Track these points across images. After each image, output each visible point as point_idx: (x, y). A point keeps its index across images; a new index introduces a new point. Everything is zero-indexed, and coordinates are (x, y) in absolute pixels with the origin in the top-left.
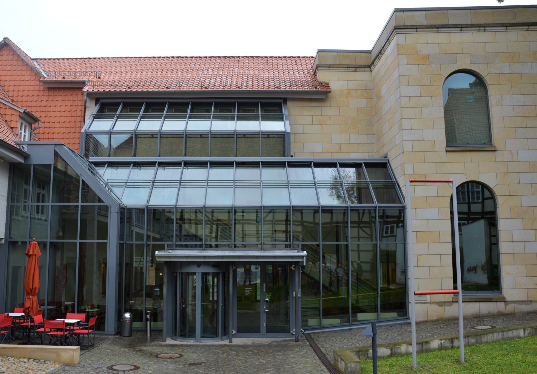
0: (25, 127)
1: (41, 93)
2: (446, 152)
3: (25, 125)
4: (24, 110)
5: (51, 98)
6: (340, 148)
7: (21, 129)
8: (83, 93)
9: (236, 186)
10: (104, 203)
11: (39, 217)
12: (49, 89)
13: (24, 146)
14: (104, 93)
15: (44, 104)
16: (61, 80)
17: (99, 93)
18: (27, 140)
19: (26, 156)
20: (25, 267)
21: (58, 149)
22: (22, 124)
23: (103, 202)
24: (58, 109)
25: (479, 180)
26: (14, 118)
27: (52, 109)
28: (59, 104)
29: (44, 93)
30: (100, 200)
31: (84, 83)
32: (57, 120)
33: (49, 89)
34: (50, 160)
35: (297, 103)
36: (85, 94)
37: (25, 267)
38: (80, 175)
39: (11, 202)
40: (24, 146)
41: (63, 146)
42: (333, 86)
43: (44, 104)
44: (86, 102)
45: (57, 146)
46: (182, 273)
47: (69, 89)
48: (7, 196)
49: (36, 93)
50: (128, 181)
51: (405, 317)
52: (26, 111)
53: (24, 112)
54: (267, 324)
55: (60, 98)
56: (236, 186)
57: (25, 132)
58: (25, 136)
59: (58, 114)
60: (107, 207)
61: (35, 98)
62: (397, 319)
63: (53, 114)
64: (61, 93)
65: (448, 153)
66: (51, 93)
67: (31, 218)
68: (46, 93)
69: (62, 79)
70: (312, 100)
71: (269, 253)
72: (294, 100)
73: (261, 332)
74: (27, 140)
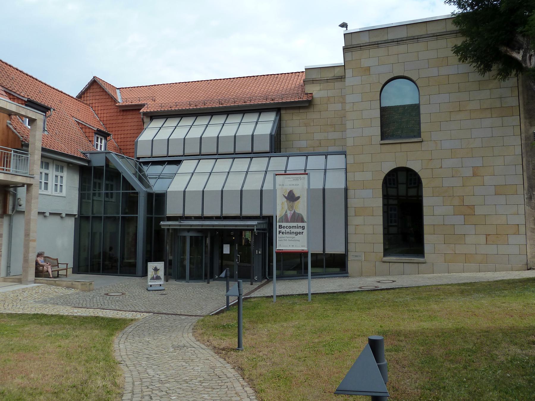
0: (101, 139)
1: (119, 114)
2: (380, 145)
3: (101, 138)
4: (97, 129)
5: (125, 117)
6: (320, 143)
7: (97, 141)
8: (140, 113)
9: (59, 177)
10: (136, 190)
11: (110, 200)
12: (123, 111)
13: (87, 154)
14: (154, 112)
15: (120, 121)
16: (129, 104)
17: (151, 112)
18: (103, 150)
19: (89, 162)
20: (100, 233)
21: (108, 156)
22: (97, 138)
23: (135, 190)
24: (129, 124)
25: (407, 166)
26: (91, 134)
27: (125, 125)
28: (130, 121)
29: (120, 114)
30: (134, 189)
31: (142, 106)
32: (129, 132)
33: (123, 111)
34: (103, 163)
35: (288, 111)
36: (142, 114)
37: (100, 233)
38: (121, 172)
39: (81, 191)
40: (87, 154)
41: (111, 153)
42: (315, 95)
43: (120, 121)
44: (143, 119)
45: (107, 154)
46: (180, 236)
47: (133, 110)
48: (78, 187)
49: (116, 114)
50: (161, 175)
51: (345, 272)
52: (98, 129)
53: (97, 130)
54: (238, 272)
55: (130, 117)
56: (59, 177)
57: (101, 142)
58: (101, 146)
59: (129, 128)
60: (137, 193)
61: (115, 118)
62: (339, 272)
63: (126, 128)
64: (131, 113)
65: (382, 146)
66: (125, 114)
67: (104, 201)
68: (122, 114)
69: (130, 104)
70: (299, 108)
71: (231, 223)
72: (286, 109)
73: (235, 277)
74: (103, 150)
